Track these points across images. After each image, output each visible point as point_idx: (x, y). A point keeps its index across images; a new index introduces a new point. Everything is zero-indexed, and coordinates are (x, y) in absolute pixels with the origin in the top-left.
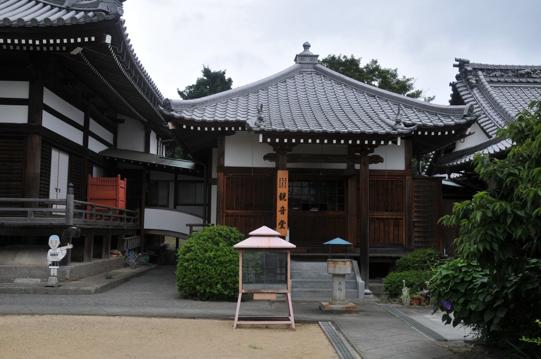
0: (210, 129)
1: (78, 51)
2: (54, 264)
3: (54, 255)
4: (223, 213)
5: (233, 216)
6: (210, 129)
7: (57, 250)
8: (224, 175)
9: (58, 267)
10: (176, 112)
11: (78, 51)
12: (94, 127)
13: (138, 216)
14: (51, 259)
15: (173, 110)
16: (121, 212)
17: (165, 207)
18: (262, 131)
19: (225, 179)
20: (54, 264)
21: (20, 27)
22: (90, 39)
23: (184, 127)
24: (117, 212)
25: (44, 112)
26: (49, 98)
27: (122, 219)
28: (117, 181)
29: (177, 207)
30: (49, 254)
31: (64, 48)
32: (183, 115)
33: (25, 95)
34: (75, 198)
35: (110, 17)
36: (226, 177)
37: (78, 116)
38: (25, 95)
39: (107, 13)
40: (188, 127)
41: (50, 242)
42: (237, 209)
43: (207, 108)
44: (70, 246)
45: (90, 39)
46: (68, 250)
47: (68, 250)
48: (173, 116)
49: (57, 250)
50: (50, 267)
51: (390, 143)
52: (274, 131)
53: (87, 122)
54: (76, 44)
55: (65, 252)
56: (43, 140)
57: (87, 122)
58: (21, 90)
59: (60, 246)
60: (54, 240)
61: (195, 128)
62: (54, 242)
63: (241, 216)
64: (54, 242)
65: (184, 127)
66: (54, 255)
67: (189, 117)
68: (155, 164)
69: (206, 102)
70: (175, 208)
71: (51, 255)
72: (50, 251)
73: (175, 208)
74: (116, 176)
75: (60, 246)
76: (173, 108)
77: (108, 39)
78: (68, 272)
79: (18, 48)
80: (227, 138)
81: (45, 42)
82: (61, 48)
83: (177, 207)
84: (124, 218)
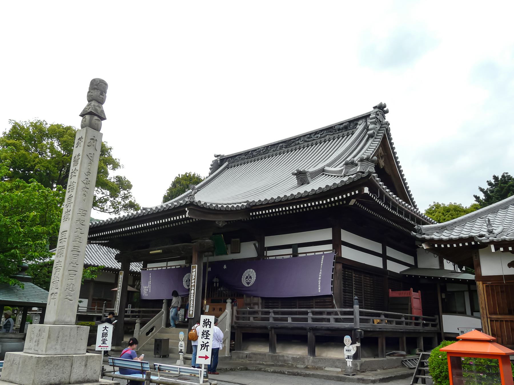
0: (458, 245)
1: (352, 202)
2: (348, 357)
3: (348, 351)
4: (487, 318)
5: (498, 321)
6: (458, 245)
7: (350, 348)
8: (483, 284)
9: (352, 360)
10: (428, 235)
11: (352, 202)
12: (391, 252)
13: (437, 321)
14: (346, 354)
15: (424, 234)
16: (417, 318)
17: (463, 313)
18: (492, 242)
19: (485, 288)
20: (348, 357)
21: (313, 194)
22: (355, 193)
23: (436, 246)
24: (413, 318)
25: (343, 247)
26: (346, 236)
27: (417, 324)
28: (410, 293)
29: (474, 313)
30: (345, 350)
31: (345, 202)
32: (433, 236)
33: (330, 237)
34: (360, 308)
35: (365, 175)
36: (484, 285)
37: (377, 247)
38: (330, 237)
39: (363, 173)
40: (439, 246)
41: (345, 341)
42: (500, 314)
43: (456, 228)
44: (358, 344)
45: (355, 193)
46: (357, 347)
47: (357, 347)
48: (424, 238)
49: (350, 348)
50: (347, 360)
51: (502, 249)
52: (504, 241)
53: (384, 250)
54: (352, 197)
55: (355, 349)
56: (343, 267)
57: (384, 250)
58: (327, 234)
59: (351, 344)
60: (347, 339)
61: (446, 246)
62: (347, 341)
63: (496, 321)
64: (347, 341)
65: (436, 246)
66: (348, 351)
67: (438, 238)
68: (444, 278)
69: (455, 223)
70: (472, 314)
71: (346, 350)
72: (345, 347)
73: (472, 315)
74: (409, 290)
75: (351, 344)
76: (423, 232)
77: (366, 190)
78: (359, 364)
79: (319, 208)
80: (480, 250)
81: (328, 200)
82: (289, 212)
83: (474, 313)
84: (403, 322)
